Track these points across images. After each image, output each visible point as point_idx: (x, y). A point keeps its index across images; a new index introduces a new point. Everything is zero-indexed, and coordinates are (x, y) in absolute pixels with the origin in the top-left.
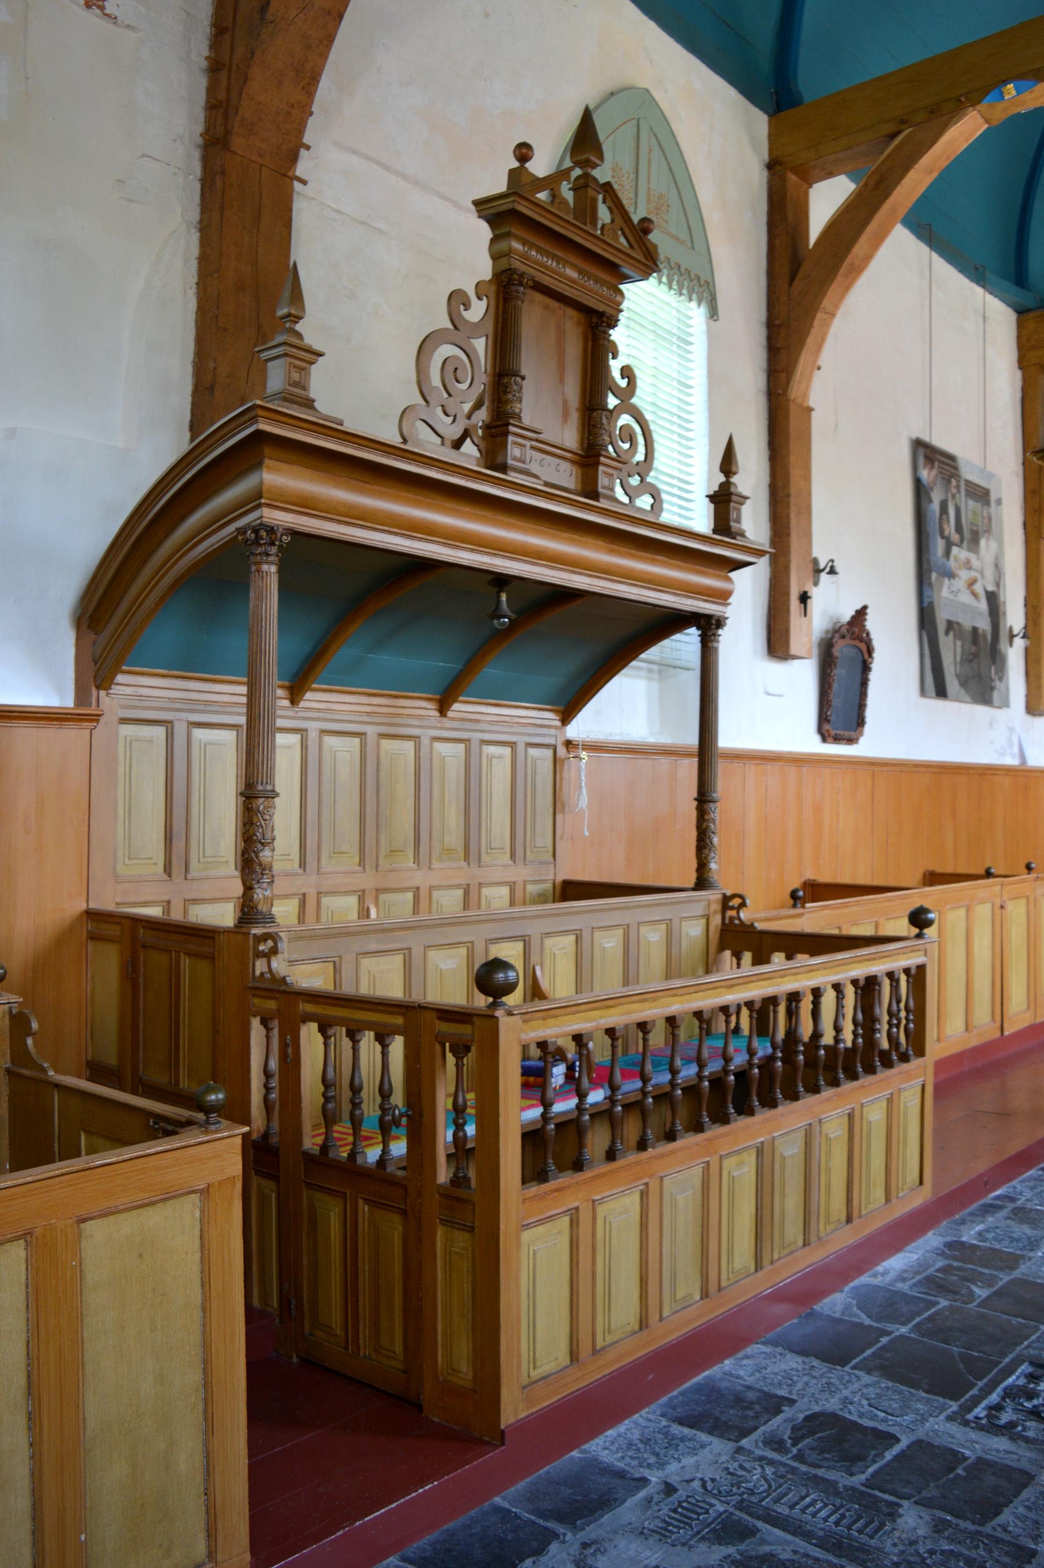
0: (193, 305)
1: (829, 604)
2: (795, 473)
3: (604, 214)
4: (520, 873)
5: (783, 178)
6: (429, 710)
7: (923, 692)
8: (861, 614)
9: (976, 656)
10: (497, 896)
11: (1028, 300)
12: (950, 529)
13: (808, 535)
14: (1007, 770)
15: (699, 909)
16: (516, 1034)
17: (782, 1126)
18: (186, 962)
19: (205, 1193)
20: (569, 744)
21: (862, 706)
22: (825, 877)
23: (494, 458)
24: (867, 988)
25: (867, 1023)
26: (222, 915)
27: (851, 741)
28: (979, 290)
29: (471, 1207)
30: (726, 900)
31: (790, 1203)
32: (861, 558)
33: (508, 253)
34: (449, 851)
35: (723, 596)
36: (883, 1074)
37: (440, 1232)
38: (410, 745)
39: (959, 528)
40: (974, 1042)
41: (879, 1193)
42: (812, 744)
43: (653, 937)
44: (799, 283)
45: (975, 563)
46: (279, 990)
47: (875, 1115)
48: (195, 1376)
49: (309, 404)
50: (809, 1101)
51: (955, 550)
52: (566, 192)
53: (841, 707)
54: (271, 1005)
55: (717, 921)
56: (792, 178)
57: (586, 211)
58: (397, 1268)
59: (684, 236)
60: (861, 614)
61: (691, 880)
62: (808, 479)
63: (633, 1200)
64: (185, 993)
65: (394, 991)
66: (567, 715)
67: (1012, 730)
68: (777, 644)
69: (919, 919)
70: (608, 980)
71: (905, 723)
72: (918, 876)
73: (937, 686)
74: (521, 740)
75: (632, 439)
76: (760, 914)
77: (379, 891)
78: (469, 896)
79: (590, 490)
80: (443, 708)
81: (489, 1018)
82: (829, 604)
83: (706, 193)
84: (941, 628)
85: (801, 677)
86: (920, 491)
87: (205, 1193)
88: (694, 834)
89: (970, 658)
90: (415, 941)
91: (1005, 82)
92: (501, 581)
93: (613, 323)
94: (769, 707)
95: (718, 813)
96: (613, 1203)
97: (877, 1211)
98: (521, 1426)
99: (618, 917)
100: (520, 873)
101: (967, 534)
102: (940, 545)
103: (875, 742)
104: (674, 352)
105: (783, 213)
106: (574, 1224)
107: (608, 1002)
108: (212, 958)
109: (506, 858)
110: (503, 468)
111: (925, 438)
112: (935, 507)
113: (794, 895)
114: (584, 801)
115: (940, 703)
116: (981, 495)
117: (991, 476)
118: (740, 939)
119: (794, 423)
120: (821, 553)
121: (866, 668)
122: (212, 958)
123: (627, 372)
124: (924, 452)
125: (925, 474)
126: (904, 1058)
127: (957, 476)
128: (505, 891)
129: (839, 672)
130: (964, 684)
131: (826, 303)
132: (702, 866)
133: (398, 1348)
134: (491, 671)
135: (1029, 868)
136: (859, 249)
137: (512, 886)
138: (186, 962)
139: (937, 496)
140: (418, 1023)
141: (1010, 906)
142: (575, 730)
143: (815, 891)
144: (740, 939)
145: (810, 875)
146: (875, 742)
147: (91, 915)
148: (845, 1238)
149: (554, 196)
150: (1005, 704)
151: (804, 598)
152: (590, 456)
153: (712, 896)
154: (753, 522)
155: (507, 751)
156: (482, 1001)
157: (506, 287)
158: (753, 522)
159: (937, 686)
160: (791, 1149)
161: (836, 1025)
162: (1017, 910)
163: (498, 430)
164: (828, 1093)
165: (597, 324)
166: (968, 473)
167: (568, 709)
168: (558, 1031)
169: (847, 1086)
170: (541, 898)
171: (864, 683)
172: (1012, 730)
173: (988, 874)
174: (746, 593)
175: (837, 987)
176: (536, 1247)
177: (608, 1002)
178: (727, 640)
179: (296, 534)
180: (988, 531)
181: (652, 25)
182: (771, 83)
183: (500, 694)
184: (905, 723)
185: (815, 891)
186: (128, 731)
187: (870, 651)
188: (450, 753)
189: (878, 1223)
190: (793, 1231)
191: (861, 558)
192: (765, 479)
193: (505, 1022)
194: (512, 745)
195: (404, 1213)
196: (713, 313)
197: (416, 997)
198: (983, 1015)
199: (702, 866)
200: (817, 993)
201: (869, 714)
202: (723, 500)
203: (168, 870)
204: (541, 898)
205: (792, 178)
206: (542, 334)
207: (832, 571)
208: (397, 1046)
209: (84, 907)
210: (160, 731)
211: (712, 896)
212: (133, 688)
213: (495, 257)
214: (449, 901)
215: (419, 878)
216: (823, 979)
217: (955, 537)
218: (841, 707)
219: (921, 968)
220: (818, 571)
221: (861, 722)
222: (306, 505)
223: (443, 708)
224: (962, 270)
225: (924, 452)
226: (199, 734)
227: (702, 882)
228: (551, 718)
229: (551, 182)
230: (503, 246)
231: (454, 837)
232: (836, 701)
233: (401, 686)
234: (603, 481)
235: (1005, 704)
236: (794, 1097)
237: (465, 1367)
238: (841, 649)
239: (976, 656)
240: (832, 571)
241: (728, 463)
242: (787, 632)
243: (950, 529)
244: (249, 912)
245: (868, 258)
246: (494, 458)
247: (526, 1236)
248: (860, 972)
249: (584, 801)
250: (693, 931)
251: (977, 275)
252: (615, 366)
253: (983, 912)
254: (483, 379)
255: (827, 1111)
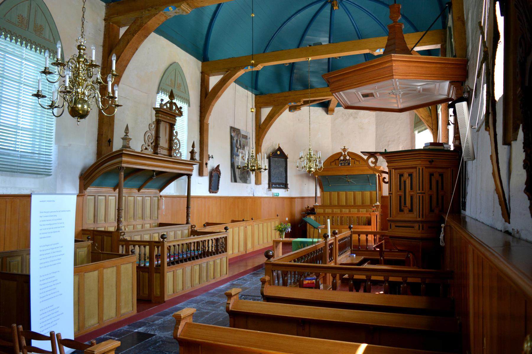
0: (98, 118)
1: (212, 164)
2: (205, 138)
3: (174, 108)
4: (151, 222)
5: (204, 76)
6: (136, 191)
7: (232, 181)
8: (218, 166)
9: (243, 173)
10: (147, 226)
11: (258, 93)
12: (238, 145)
13: (207, 151)
14: (250, 197)
15: (187, 228)
16: (166, 245)
17: (203, 261)
18: (105, 237)
19: (133, 263)
20: (161, 196)
21: (218, 185)
22: (210, 222)
23: (155, 153)
24: (217, 240)
25: (217, 246)
26: (112, 229)
27: (216, 193)
28: (246, 91)
29: (160, 269)
30: (192, 226)
31: (204, 274)
32: (219, 156)
33: (159, 116)
34: (139, 218)
35: (192, 170)
36: (219, 255)
37: (155, 274)
38: (133, 198)
39: (240, 145)
40: (240, 254)
41: (219, 275)
42: (207, 193)
43: (179, 233)
44: (207, 98)
45: (244, 152)
46: (125, 241)
47: (218, 261)
48: (131, 286)
49: (129, 148)
50: (207, 258)
51: (239, 150)
52: (168, 105)
53: (214, 186)
54: (124, 243)
55: (190, 230)
56: (206, 76)
57: (171, 107)
58: (147, 281)
59: (184, 91)
60: (218, 166)
61: (185, 223)
62: (208, 139)
63: (181, 270)
64: (105, 243)
65: (148, 240)
66: (160, 191)
67: (252, 188)
68: (201, 173)
69: (226, 229)
70: (179, 237)
71: (228, 188)
72: (230, 221)
73: (234, 179)
74: (152, 196)
75: (177, 145)
76: (198, 229)
77: (128, 225)
78: (143, 226)
79: (170, 155)
80: (139, 190)
81: (163, 242)
82: (212, 164)
83: (188, 81)
84: (236, 167)
85: (205, 180)
86: (232, 138)
87: (133, 263)
88: (186, 214)
89: (242, 173)
90: (142, 233)
91: (248, 66)
92: (154, 171)
93: (174, 125)
94: (200, 186)
95: (191, 210)
96: (179, 270)
97: (219, 278)
98: (167, 301)
99: (173, 229)
100: (151, 222)
101: (242, 146)
102: (236, 149)
103: (222, 192)
104: (184, 129)
105: (204, 83)
106: (174, 273)
107: (179, 240)
108: (111, 236)
109: (149, 219)
110: (157, 154)
111: (233, 126)
112: (235, 141)
113: (204, 225)
114: (164, 207)
115: (235, 183)
116: (245, 137)
117: (248, 133)
118: (194, 233)
119: (205, 128)
120: (210, 153)
121: (219, 177)
122: (111, 236)
123: (176, 132)
124: (233, 129)
125: (233, 134)
126: (223, 252)
127: (240, 134)
128: (149, 225)
129: (214, 178)
130: (241, 179)
131: (212, 104)
132: (187, 220)
133: (147, 293)
134: (149, 184)
135: (252, 219)
136: (219, 94)
137: (150, 224)
138: (105, 237)
139: (235, 139)
140: (151, 244)
141: (248, 227)
142: (161, 194)
143: (208, 224)
144: (194, 233)
145: (207, 221)
146: (220, 193)
147: (83, 230)
148: (213, 281)
149: (167, 106)
150: (250, 183)
151: (206, 164)
152: (170, 149)
153: (189, 225)
154: (197, 157)
155: (149, 198)
156: (162, 240)
157: (158, 122)
158: (197, 157)
159: (234, 179)
160: (204, 265)
161: (211, 247)
162: (249, 228)
163: (156, 146)
164: (210, 257)
165: (172, 126)
166: (243, 133)
167: (161, 190)
168: (171, 244)
169: (213, 256)
170: (155, 226)
171: (219, 180)
172: (252, 188)
173: (243, 220)
174: (196, 168)
175: (212, 240)
176: (169, 276)
177: (179, 240)
178: (192, 178)
179: (126, 167)
180: (247, 145)
181: (179, 48)
182: (203, 56)
183: (149, 188)
184: (228, 188)
185: (208, 224)
186: (89, 197)
187: (220, 173)
188: (140, 199)
189: (219, 280)
190: (205, 279)
191: (219, 156)
192: (199, 139)
193: (165, 243)
194: (151, 197)
195: (148, 272)
196: (189, 106)
197: (152, 240)
198: (242, 249)
199: (187, 220)
200: (208, 240)
201: (220, 187)
202: (192, 153)
203: (94, 222)
204: (155, 226)
205: (206, 76)
206: (164, 128)
207: (212, 158)
208: (147, 248)
209: (81, 229)
210: (93, 197)
211: (189, 225)
212: (91, 190)
213: (156, 116)
214: (139, 227)
215: (134, 223)
216: (210, 238)
217: (239, 147)
218: (214, 186)
219: (226, 237)
220: (209, 157)
221: (218, 189)
222: (128, 162)
223: (139, 190)
224: (243, 87)
225: (233, 129)
226: (99, 197)
227: (187, 223)
228: (158, 191)
229: (166, 104)
230: (157, 115)
231: (140, 215)
232: (213, 185)
233: (132, 187)
234: (172, 153)
235: (250, 183)
236: (205, 257)
237: (159, 293)
238: (214, 174)
239: (243, 173)
240: (212, 158)
241: (193, 146)
242: (203, 171)
243: (238, 145)
244: (119, 229)
245: (221, 95)
246: (155, 153)
247: (168, 274)
248: (216, 237)
249: (164, 207)
250: (186, 232)
251: (246, 88)
252: (174, 132)
253: (242, 228)
254: (154, 138)
255: (210, 260)
